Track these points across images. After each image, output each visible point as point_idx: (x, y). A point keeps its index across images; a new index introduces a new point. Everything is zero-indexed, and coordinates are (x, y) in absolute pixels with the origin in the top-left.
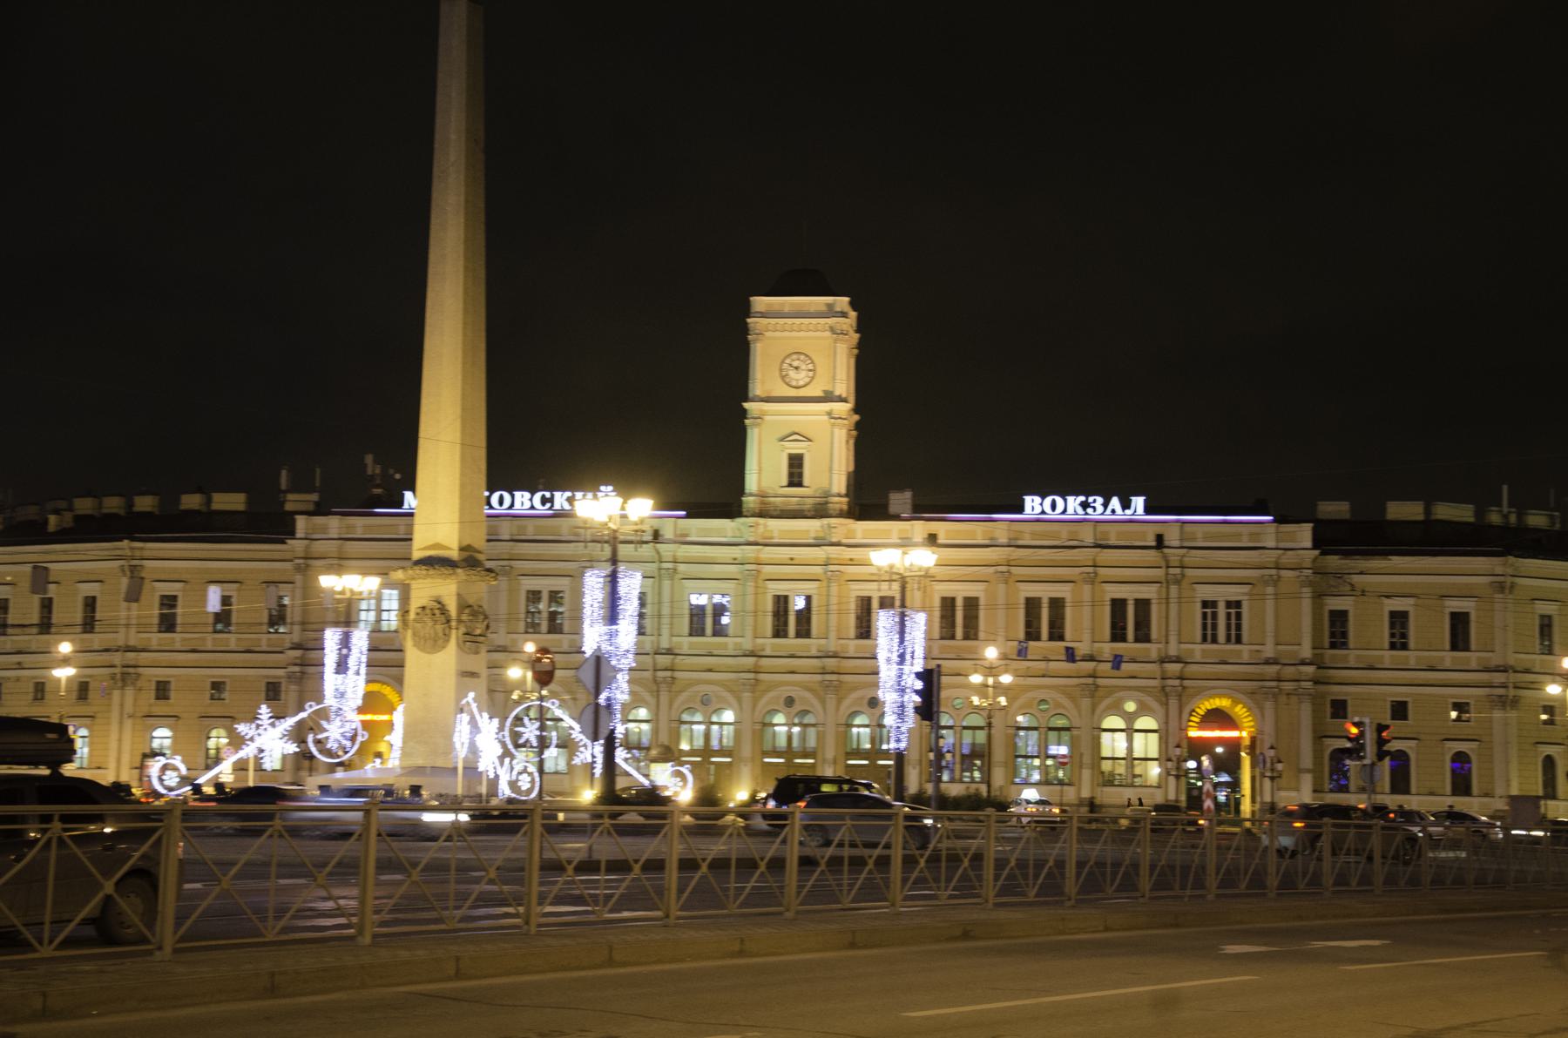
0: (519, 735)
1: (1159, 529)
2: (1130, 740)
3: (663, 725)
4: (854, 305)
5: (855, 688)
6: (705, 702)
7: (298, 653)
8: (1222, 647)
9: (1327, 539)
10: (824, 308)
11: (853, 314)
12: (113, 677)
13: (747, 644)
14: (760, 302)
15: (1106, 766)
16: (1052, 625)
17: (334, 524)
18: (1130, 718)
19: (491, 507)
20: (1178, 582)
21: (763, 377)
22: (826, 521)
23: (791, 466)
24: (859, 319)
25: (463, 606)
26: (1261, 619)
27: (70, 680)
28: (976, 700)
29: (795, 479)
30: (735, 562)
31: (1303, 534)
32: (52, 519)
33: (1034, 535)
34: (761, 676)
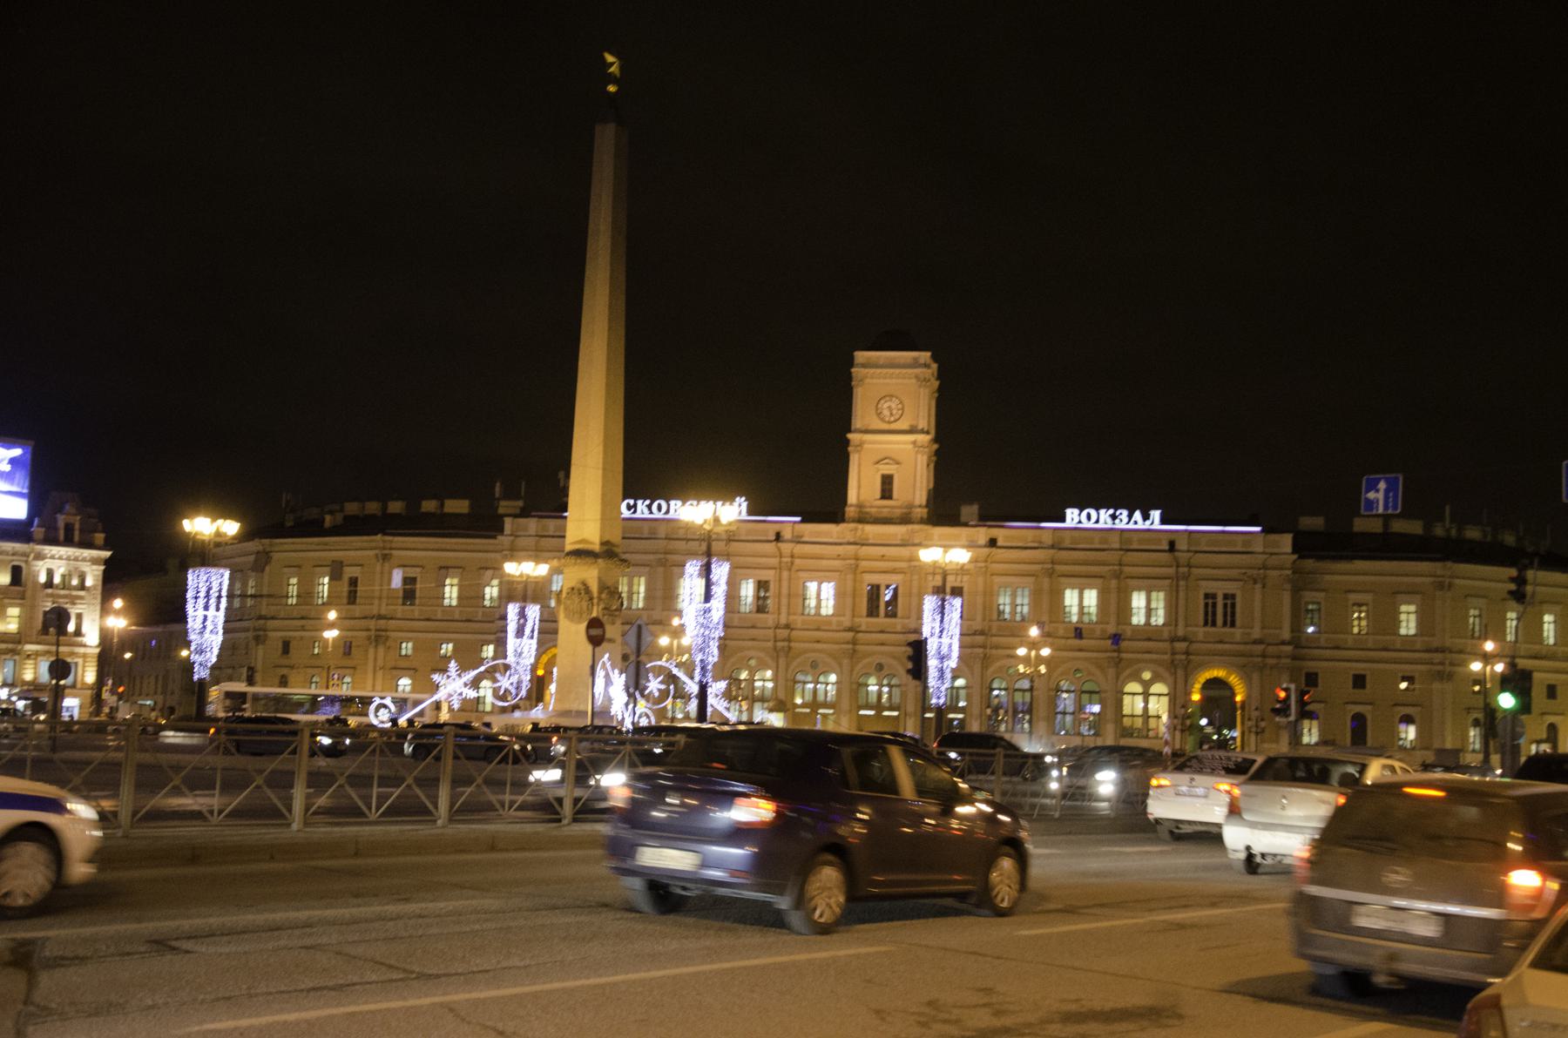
1: (777, 527)
2: (1146, 702)
3: (781, 681)
4: (935, 358)
6: (814, 665)
7: (851, 634)
8: (1219, 630)
9: (1305, 546)
12: (369, 638)
14: (861, 356)
15: (1127, 722)
17: (532, 524)
18: (1147, 685)
20: (1186, 577)
21: (862, 414)
22: (910, 527)
24: (939, 369)
25: (603, 587)
26: (1251, 605)
27: (335, 640)
28: (1021, 669)
29: (887, 493)
30: (838, 557)
32: (328, 518)
33: (1140, 541)
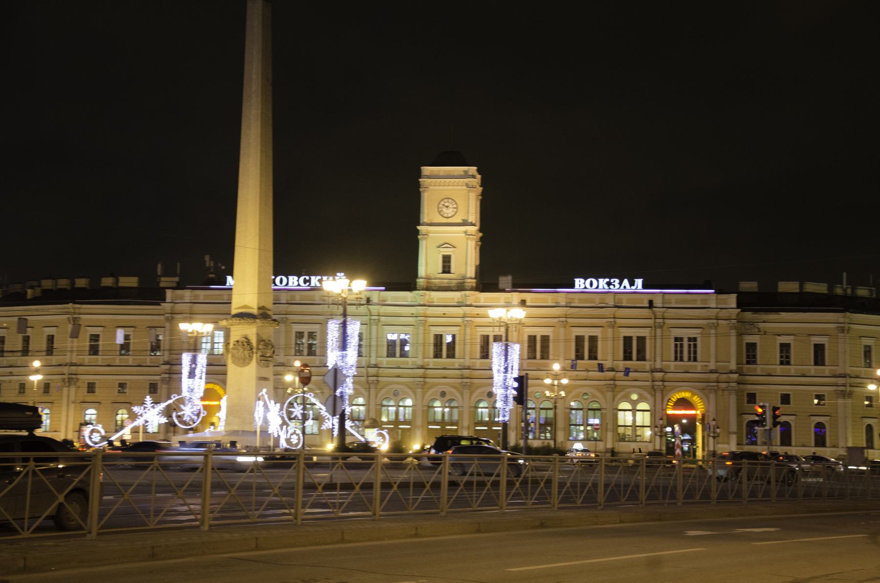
0: (291, 413)
1: (650, 297)
5: (480, 387)
8: (686, 364)
10: (462, 173)
11: (479, 176)
13: (419, 361)
14: (427, 170)
16: (590, 351)
19: (276, 285)
23: (444, 262)
29: (446, 269)
30: (412, 316)
31: (732, 300)
33: (580, 300)
34: (427, 380)
